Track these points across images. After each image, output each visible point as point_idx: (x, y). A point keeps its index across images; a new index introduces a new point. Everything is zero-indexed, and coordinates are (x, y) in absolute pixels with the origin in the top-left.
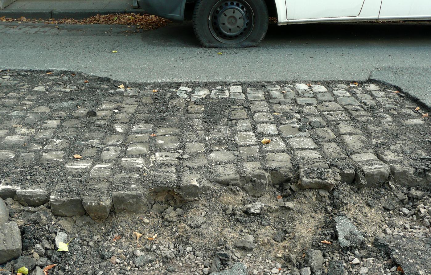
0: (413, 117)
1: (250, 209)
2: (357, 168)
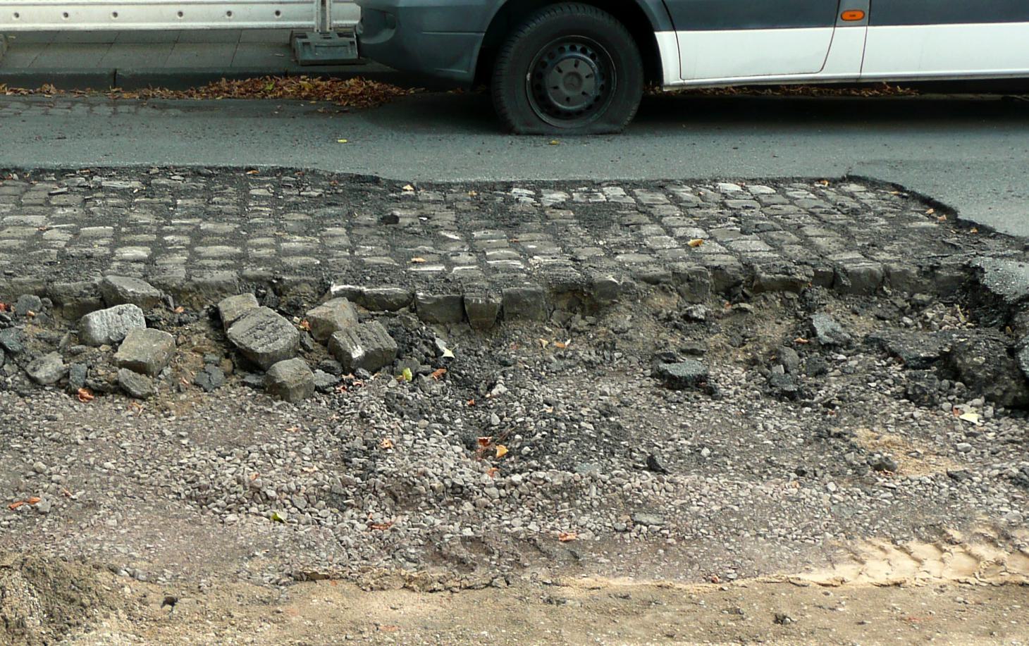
0: (922, 220)
1: (691, 311)
2: (835, 266)
